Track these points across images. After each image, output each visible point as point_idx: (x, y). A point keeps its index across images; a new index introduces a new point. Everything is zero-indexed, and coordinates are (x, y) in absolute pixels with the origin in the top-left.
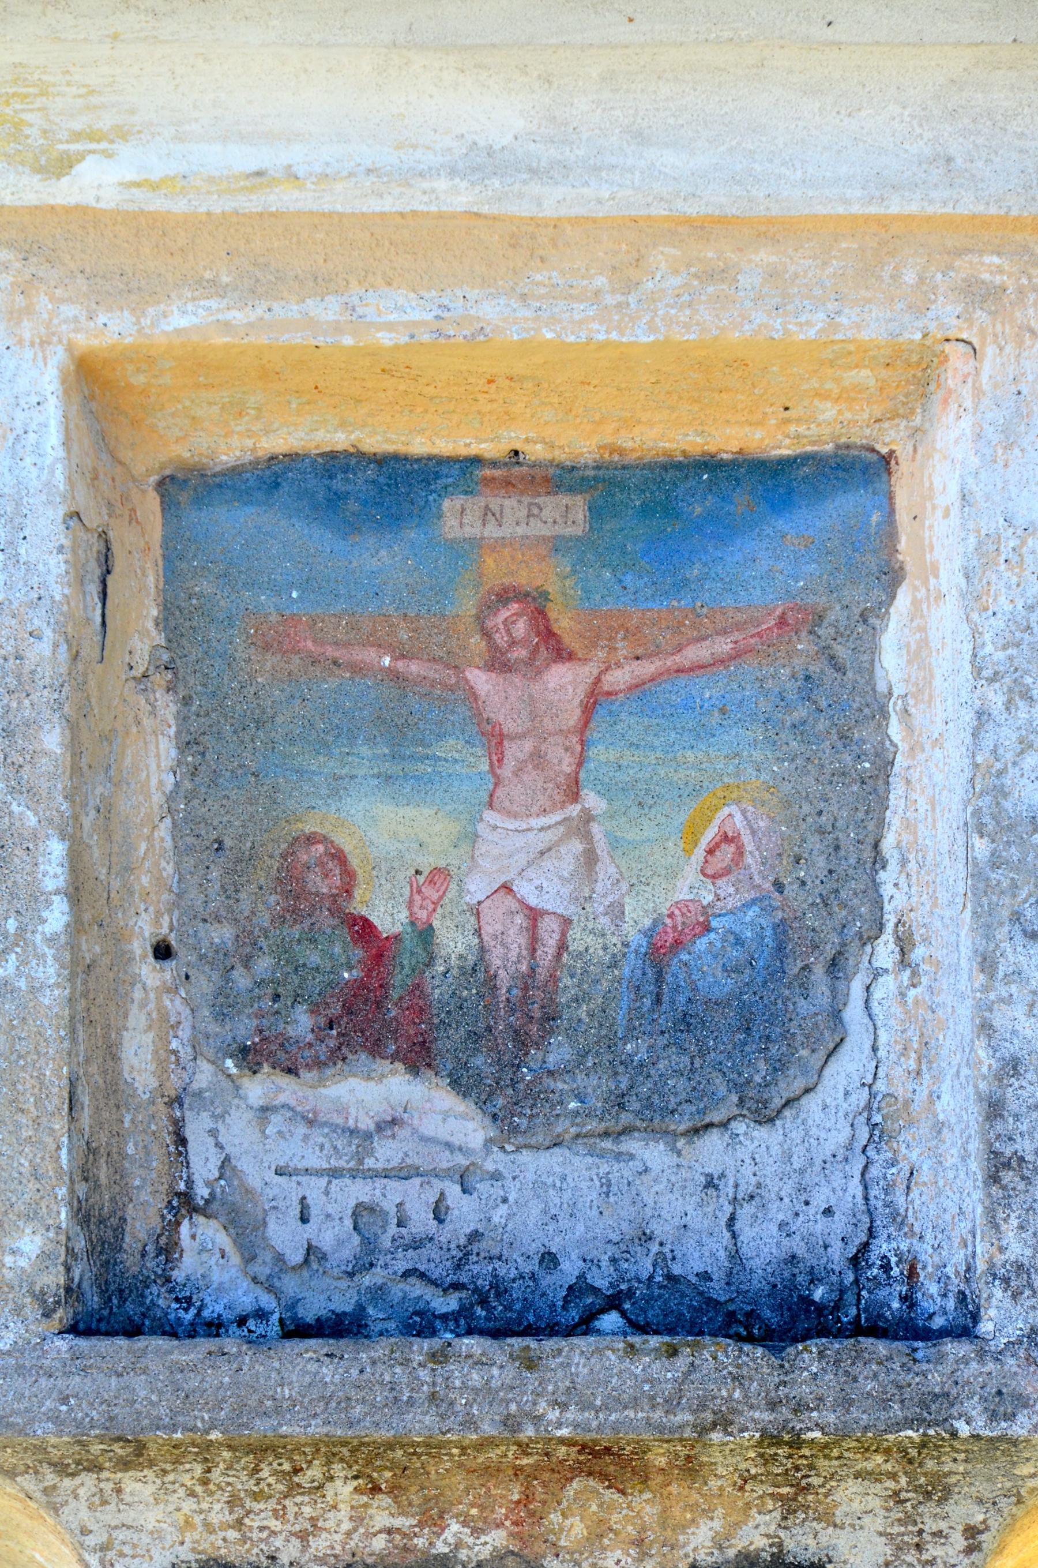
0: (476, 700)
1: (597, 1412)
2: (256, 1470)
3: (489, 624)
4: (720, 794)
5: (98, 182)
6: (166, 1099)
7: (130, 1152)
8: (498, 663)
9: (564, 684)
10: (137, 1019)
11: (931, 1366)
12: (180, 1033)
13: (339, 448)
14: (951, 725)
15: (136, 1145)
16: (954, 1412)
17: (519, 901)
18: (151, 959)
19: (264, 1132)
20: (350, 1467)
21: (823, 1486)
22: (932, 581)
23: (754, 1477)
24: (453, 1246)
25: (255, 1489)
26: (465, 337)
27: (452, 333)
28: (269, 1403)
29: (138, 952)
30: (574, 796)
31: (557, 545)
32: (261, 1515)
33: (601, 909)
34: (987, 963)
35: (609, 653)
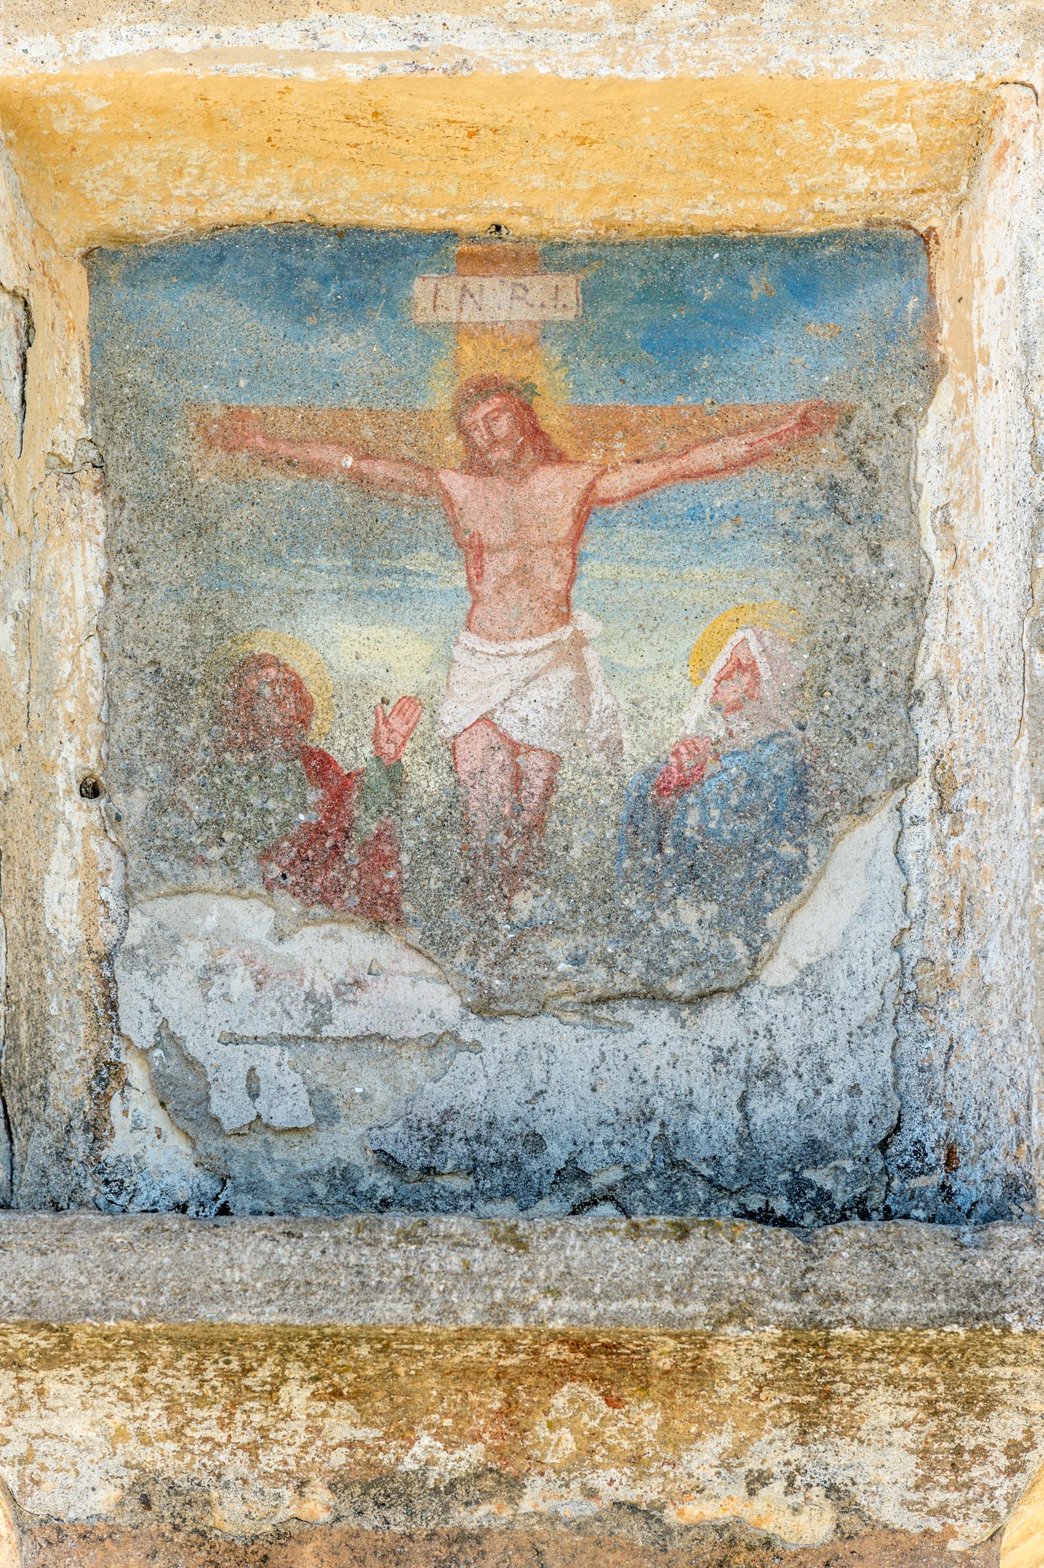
0: (452, 506)
1: (595, 1300)
2: (199, 1369)
3: (467, 420)
4: (732, 616)
6: (95, 956)
7: (52, 1012)
8: (477, 465)
9: (554, 490)
10: (60, 863)
11: (981, 1252)
12: (110, 882)
13: (295, 217)
14: (1004, 529)
15: (60, 1004)
16: (1007, 1304)
17: (500, 735)
18: (77, 796)
19: (205, 995)
20: (308, 1367)
21: (849, 1394)
22: (981, 369)
23: (770, 1383)
24: (424, 1124)
25: (197, 1392)
26: (445, 71)
27: (430, 65)
28: (216, 1287)
29: (62, 786)
30: (565, 618)
31: (543, 331)
33: (595, 745)
35: (605, 455)
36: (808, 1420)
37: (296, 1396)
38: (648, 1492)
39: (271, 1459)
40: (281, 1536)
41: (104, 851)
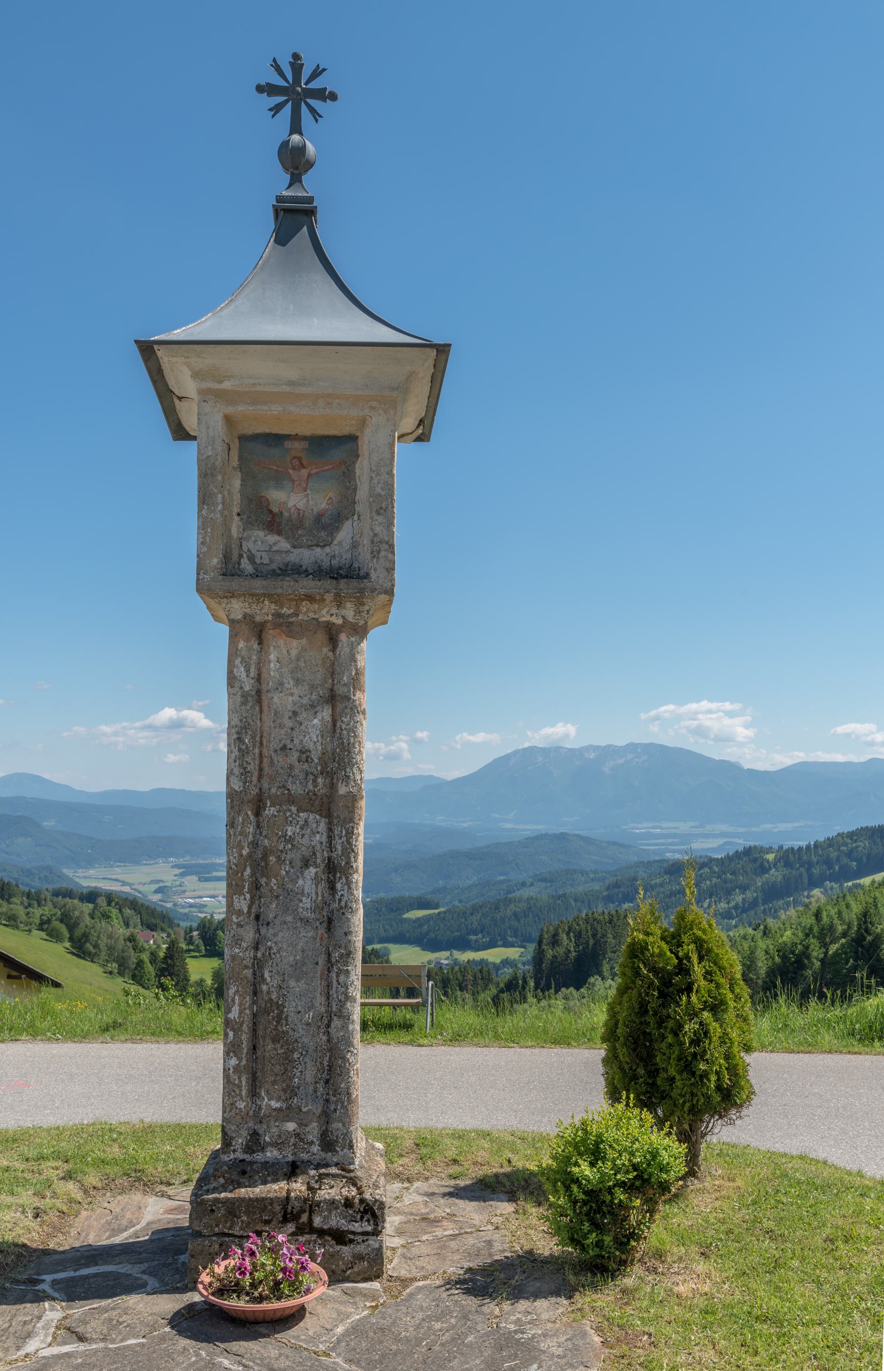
5: (227, 385)
8: (294, 469)
9: (304, 472)
32: (254, 606)
34: (372, 518)
36: (339, 607)
37: (266, 602)
38: (316, 616)
39: (263, 611)
40: (265, 622)
41: (240, 524)
